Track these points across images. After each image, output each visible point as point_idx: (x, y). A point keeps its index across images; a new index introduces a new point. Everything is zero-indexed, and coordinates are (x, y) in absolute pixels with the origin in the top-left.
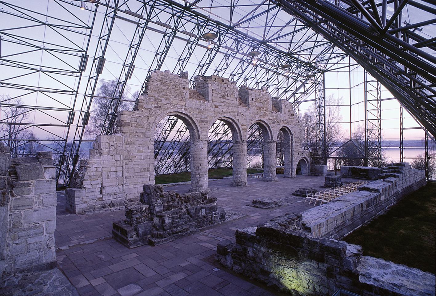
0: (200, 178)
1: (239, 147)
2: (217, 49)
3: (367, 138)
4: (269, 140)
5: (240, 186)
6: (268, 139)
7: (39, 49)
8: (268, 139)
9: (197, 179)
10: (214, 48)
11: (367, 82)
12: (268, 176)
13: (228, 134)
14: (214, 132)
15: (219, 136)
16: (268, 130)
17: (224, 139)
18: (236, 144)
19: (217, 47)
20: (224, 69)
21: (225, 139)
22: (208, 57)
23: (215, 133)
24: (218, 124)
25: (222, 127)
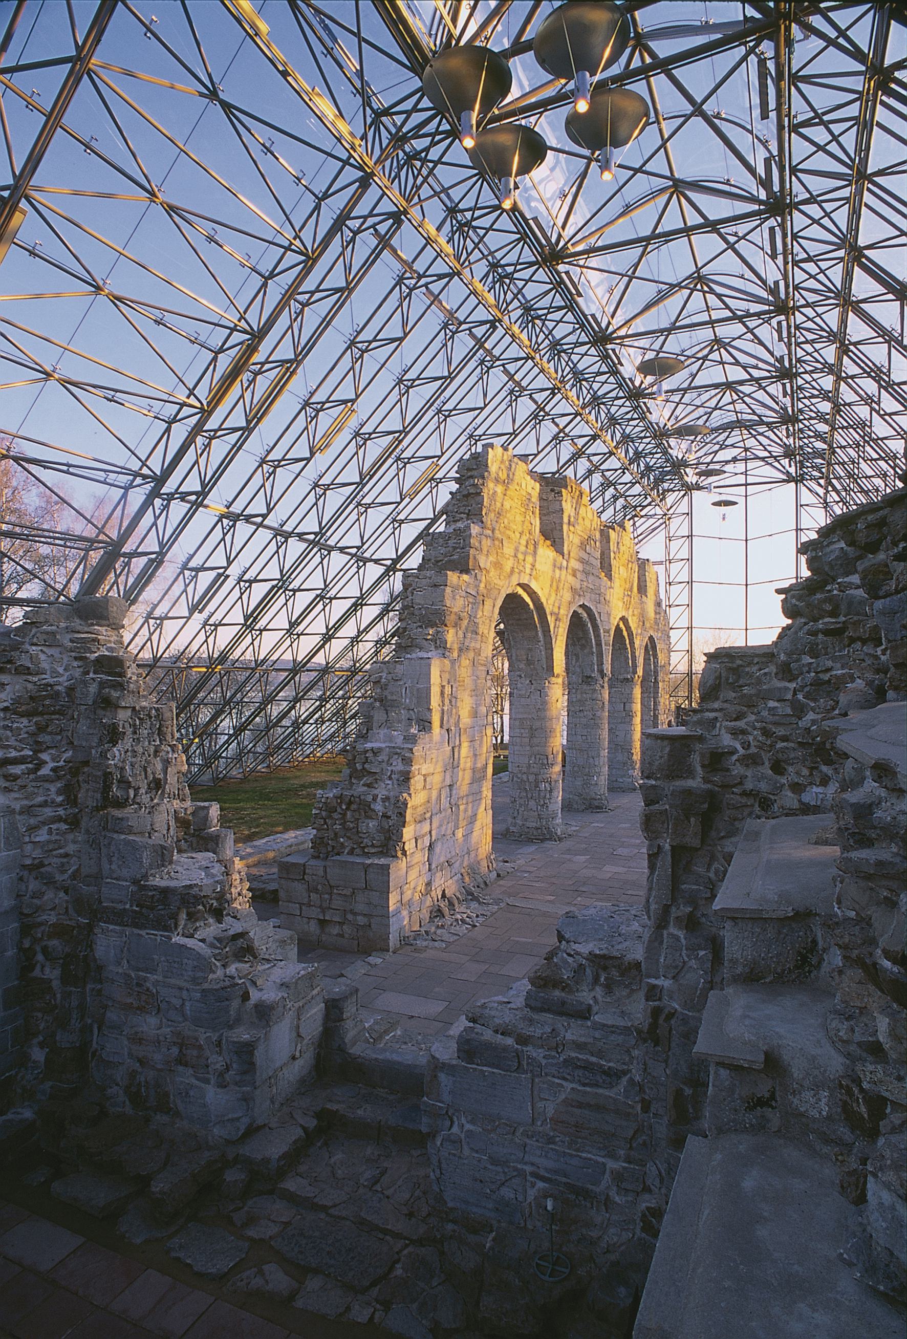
0: (551, 791)
1: (595, 696)
2: (382, 228)
3: (294, 661)
4: (628, 673)
5: (597, 807)
6: (623, 670)
7: (724, 298)
8: (623, 670)
9: (542, 794)
10: (371, 215)
11: (801, 530)
12: (622, 777)
13: (261, 631)
14: (199, 618)
15: (225, 636)
16: (628, 646)
17: (244, 652)
18: (585, 687)
19: (390, 215)
20: (393, 340)
21: (249, 655)
22: (342, 253)
23: (205, 624)
24: (319, 592)
25: (236, 593)
